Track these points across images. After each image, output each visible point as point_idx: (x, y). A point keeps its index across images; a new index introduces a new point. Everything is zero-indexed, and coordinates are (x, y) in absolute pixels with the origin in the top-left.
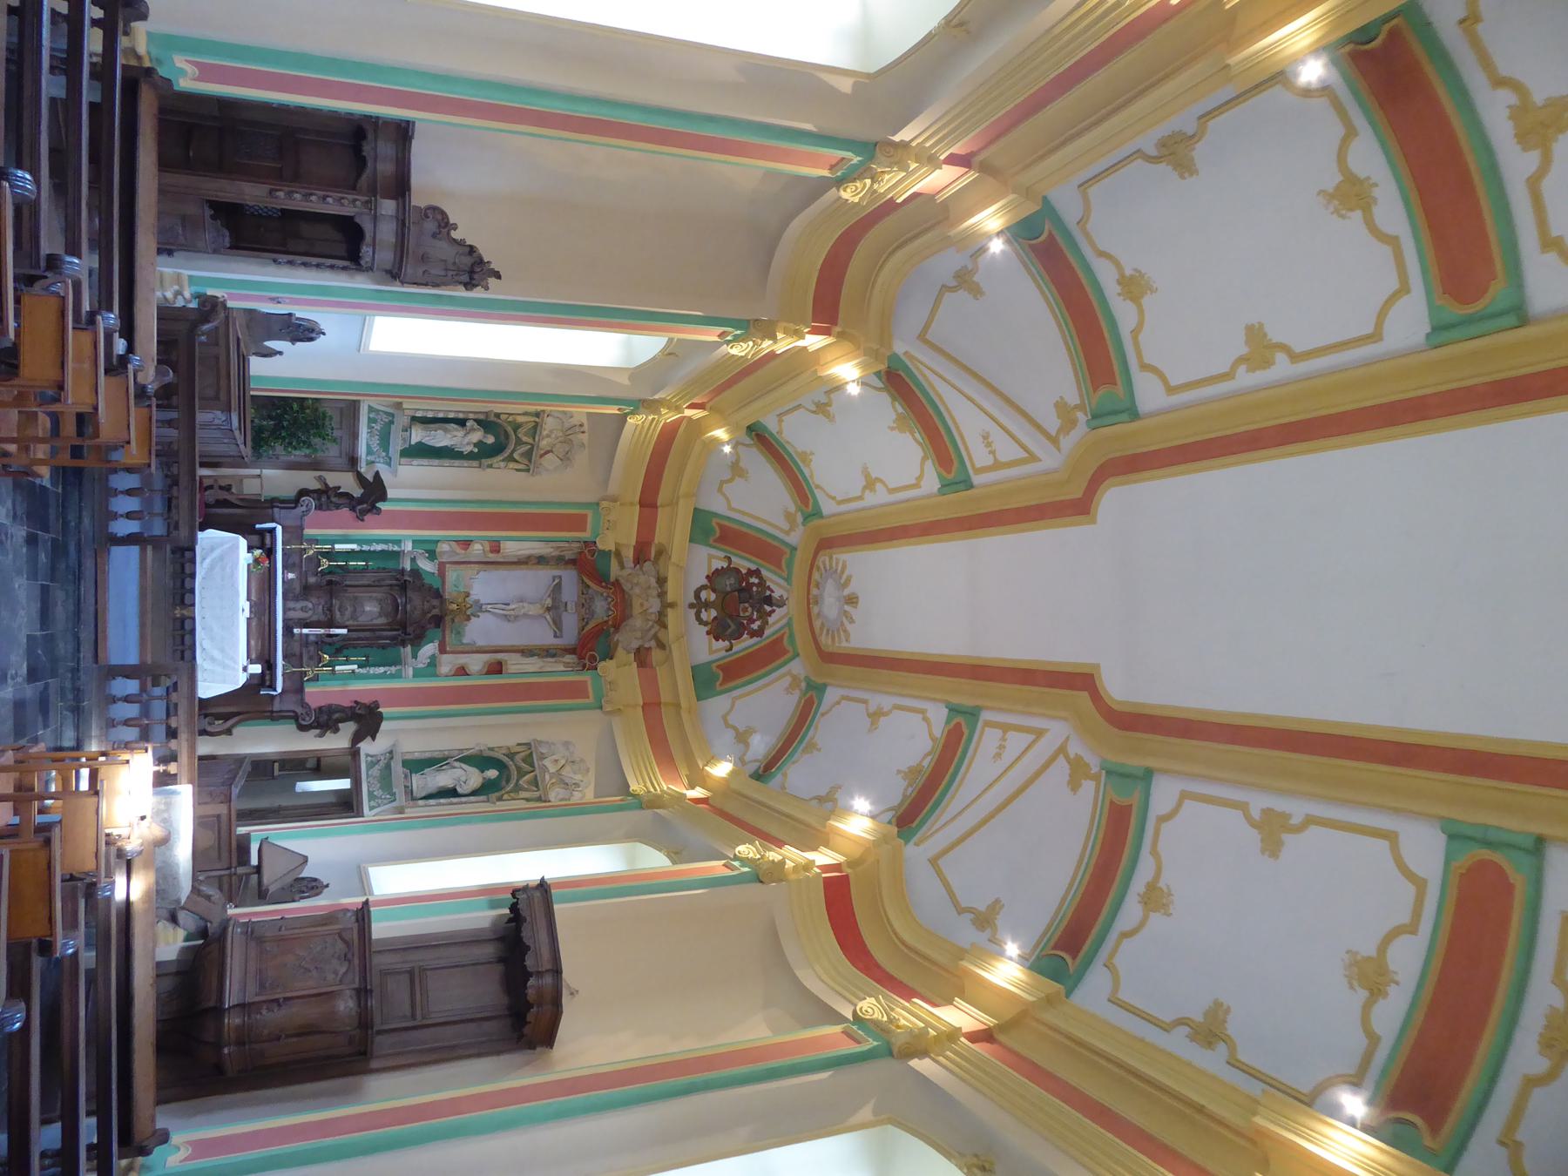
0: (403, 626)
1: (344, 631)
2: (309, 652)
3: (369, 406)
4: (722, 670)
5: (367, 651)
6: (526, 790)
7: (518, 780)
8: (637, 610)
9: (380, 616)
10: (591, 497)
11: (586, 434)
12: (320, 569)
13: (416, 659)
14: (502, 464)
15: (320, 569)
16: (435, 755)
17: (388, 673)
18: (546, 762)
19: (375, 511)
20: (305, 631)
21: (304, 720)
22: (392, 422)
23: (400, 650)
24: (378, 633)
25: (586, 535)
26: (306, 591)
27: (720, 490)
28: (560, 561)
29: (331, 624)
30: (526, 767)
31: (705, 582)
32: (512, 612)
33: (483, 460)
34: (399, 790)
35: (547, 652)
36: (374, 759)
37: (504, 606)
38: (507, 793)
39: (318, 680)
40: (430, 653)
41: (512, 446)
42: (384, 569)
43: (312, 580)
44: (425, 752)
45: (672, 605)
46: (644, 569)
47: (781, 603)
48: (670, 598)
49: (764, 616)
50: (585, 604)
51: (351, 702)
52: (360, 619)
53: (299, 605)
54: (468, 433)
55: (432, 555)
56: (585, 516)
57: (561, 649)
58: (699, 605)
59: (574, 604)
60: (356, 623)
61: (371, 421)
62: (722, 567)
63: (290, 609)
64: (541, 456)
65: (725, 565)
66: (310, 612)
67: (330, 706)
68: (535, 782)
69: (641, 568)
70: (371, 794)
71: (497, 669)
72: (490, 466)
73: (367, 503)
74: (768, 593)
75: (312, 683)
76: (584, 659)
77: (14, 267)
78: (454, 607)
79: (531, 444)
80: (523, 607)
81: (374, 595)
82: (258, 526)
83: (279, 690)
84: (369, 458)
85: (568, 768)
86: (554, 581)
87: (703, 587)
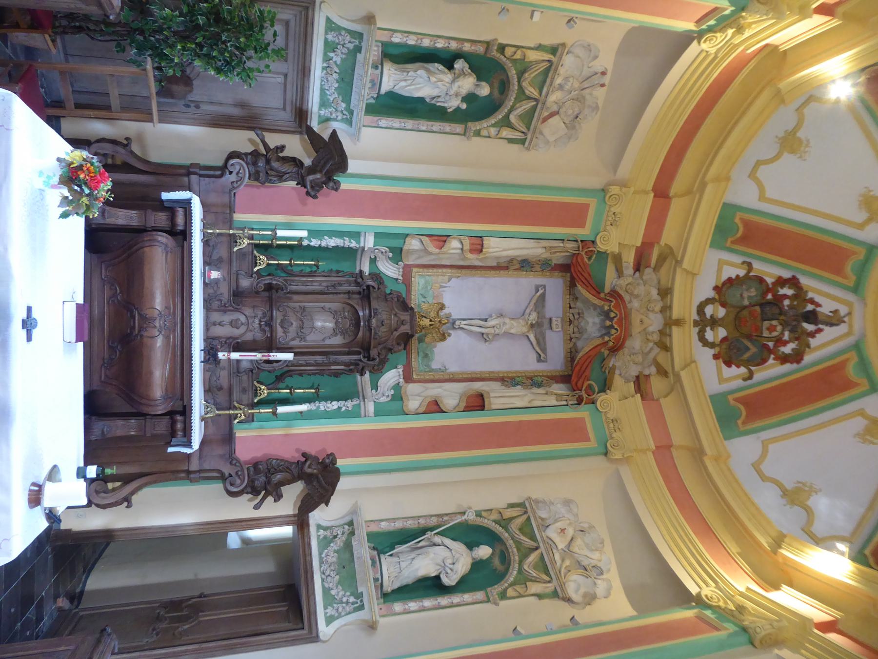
0: (366, 348)
1: (289, 356)
2: (240, 382)
3: (328, 20)
4: (744, 404)
5: (317, 379)
6: (535, 580)
7: (521, 563)
8: (636, 328)
9: (335, 334)
10: (595, 182)
11: (605, 89)
12: (256, 269)
13: (377, 390)
14: (493, 131)
15: (256, 269)
16: (410, 524)
17: (344, 409)
18: (552, 533)
19: (331, 184)
20: (235, 356)
21: (232, 485)
22: (358, 49)
23: (355, 378)
24: (333, 358)
25: (584, 233)
26: (238, 296)
27: (753, 175)
28: (546, 266)
29: (270, 345)
30: (528, 543)
31: (711, 294)
32: (491, 331)
33: (469, 124)
34: (368, 589)
35: (532, 381)
36: (328, 533)
37: (482, 323)
38: (511, 585)
39: (253, 421)
40: (392, 382)
41: (509, 103)
42: (338, 272)
43: (245, 283)
44: (394, 520)
45: (678, 323)
46: (644, 278)
47: (834, 320)
48: (676, 314)
49: (802, 338)
50: (572, 320)
51: (297, 450)
52: (308, 338)
53: (227, 318)
54: (458, 77)
55: (397, 254)
56: (586, 207)
57: (547, 377)
58: (703, 323)
59: (559, 320)
60: (303, 343)
61: (330, 47)
62: (738, 276)
63: (214, 324)
64: (545, 120)
65: (742, 273)
66: (242, 329)
67: (268, 460)
68: (543, 566)
69: (641, 277)
70: (326, 591)
71: (477, 403)
72: (478, 133)
73: (321, 172)
74: (810, 307)
75: (246, 425)
76: (581, 390)
77: (205, 226)
78: (426, 322)
79: (536, 100)
80: (504, 324)
81: (328, 305)
82: (165, 196)
83: (196, 444)
84: (322, 112)
85: (578, 542)
86: (537, 291)
87: (709, 301)
